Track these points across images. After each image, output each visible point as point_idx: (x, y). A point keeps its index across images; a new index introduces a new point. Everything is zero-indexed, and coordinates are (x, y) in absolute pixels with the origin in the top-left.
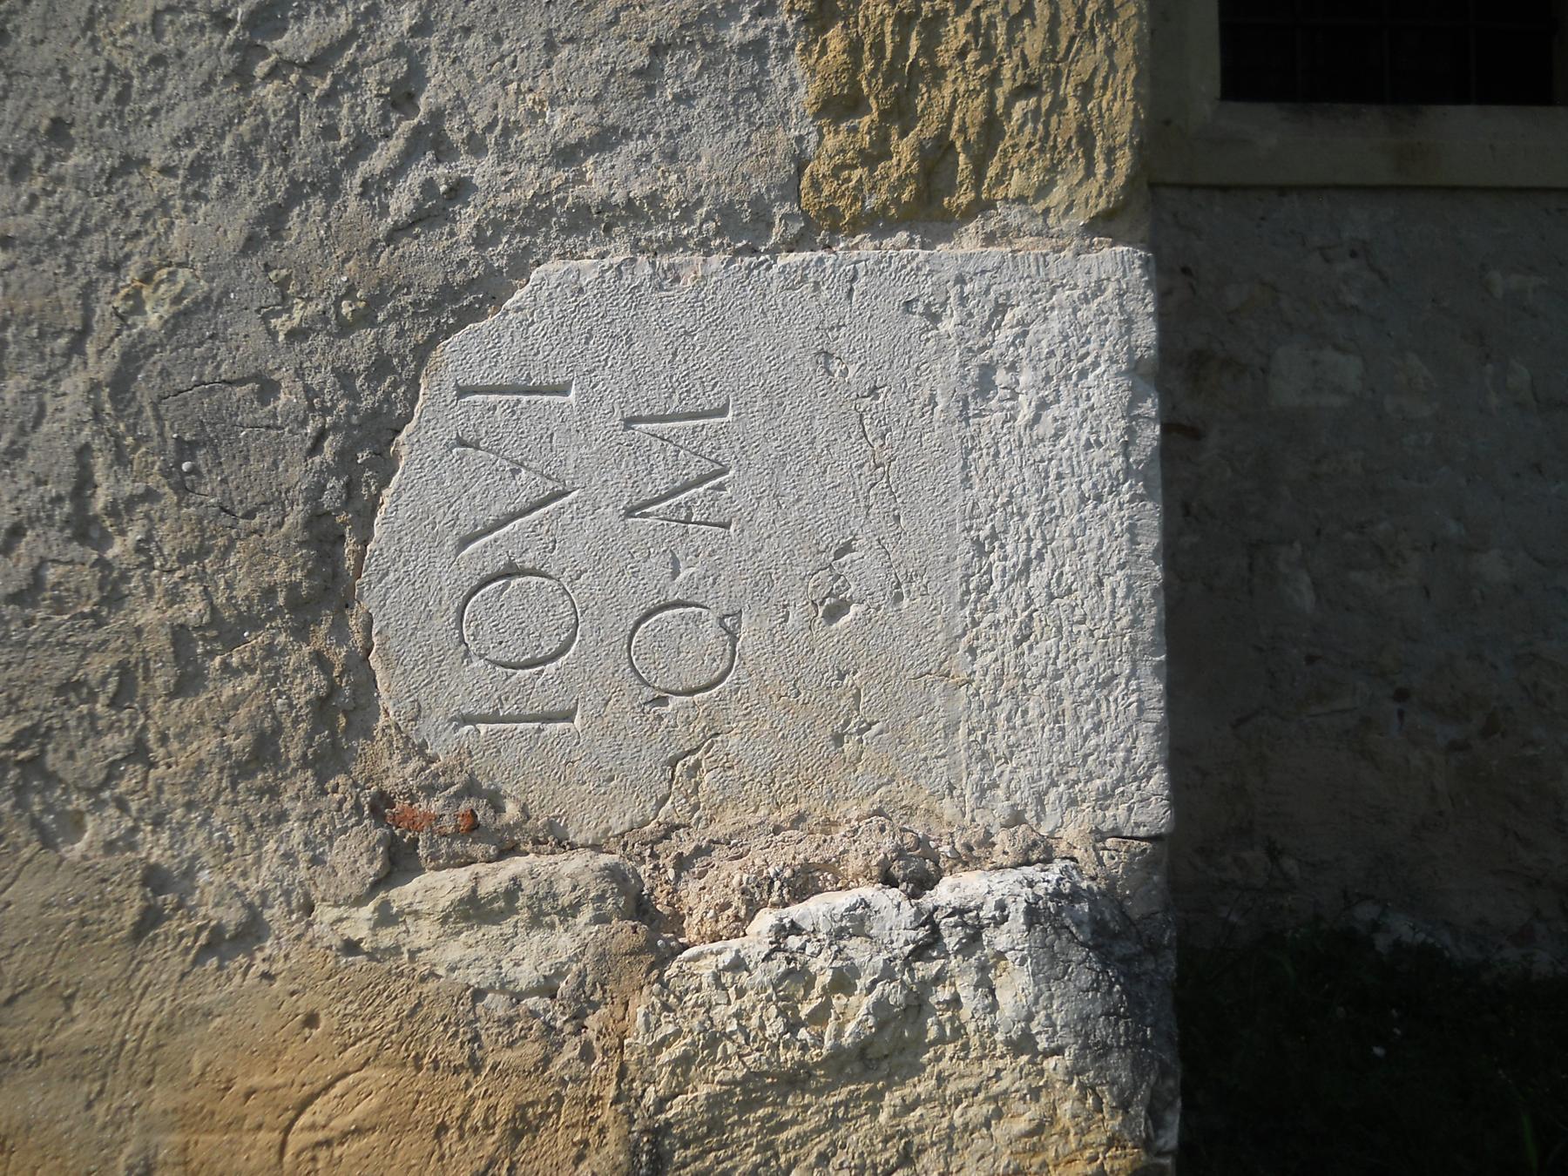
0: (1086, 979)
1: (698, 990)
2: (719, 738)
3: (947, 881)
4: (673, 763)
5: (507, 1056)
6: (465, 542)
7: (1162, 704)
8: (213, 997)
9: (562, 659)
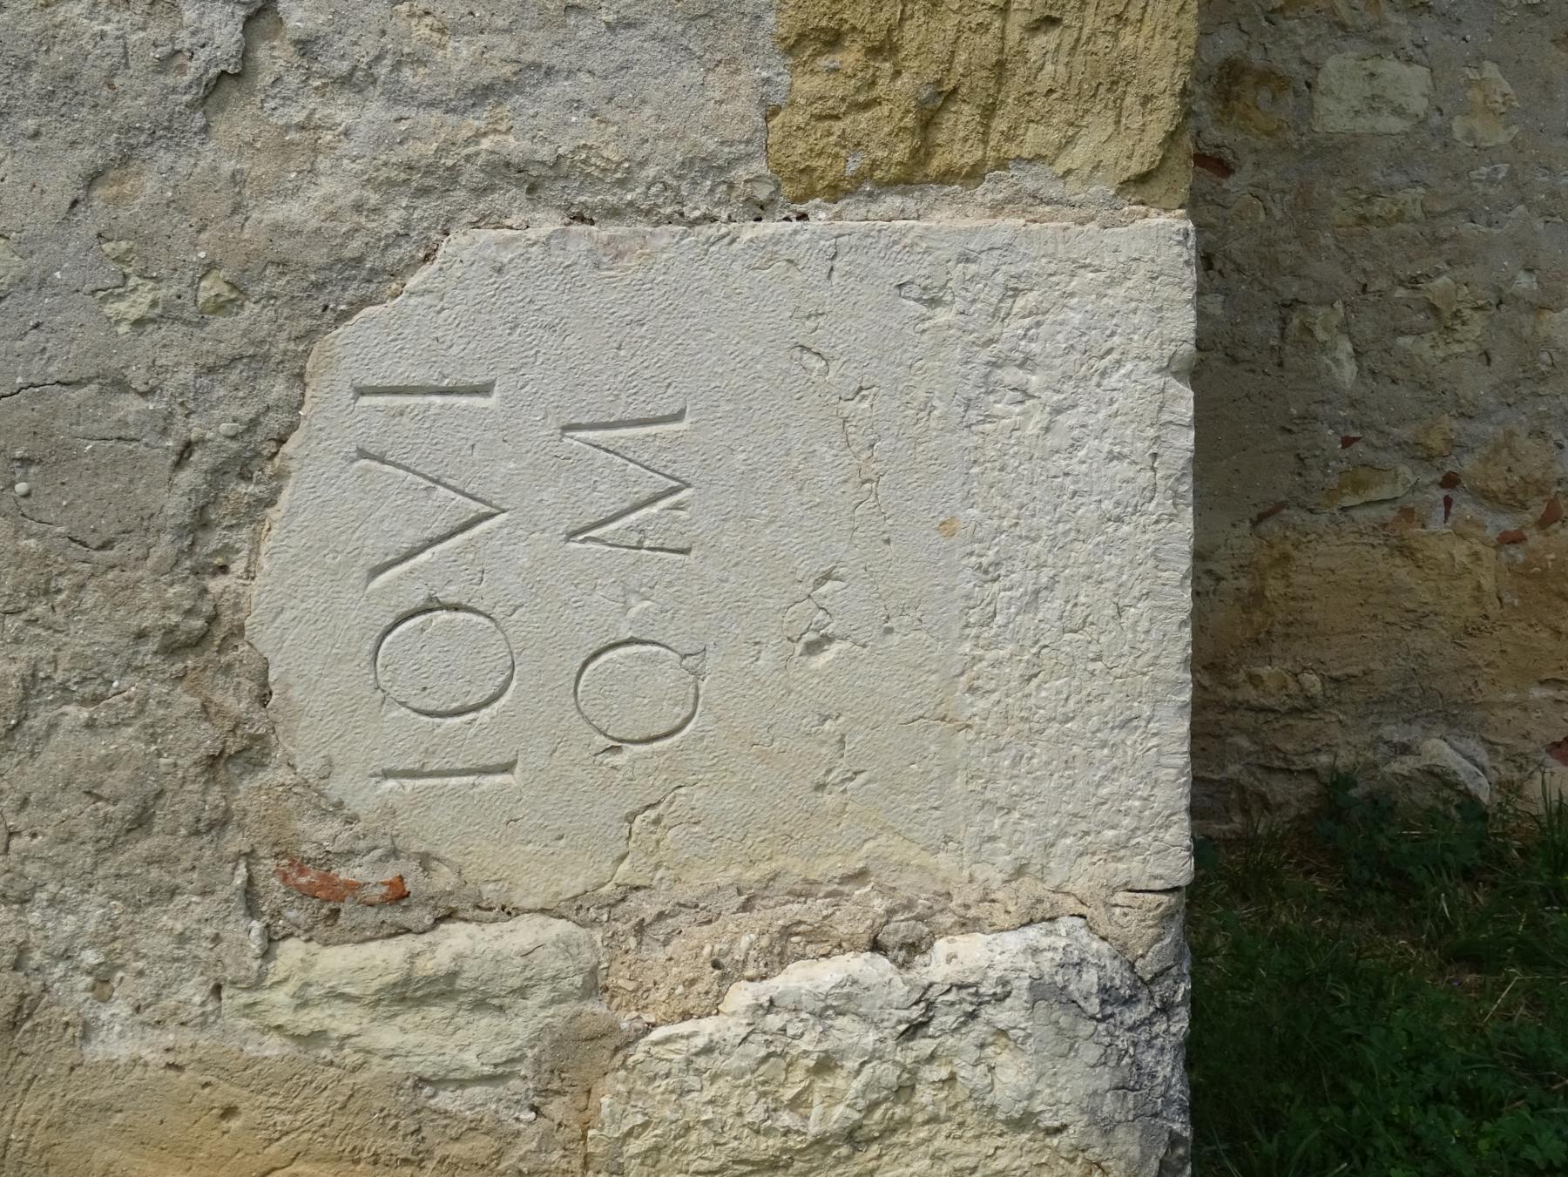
0: (1092, 1053)
1: (667, 1076)
2: (683, 791)
3: (941, 946)
4: (630, 818)
5: (456, 1149)
6: (376, 572)
7: (1185, 748)
8: (109, 1093)
9: (496, 705)
